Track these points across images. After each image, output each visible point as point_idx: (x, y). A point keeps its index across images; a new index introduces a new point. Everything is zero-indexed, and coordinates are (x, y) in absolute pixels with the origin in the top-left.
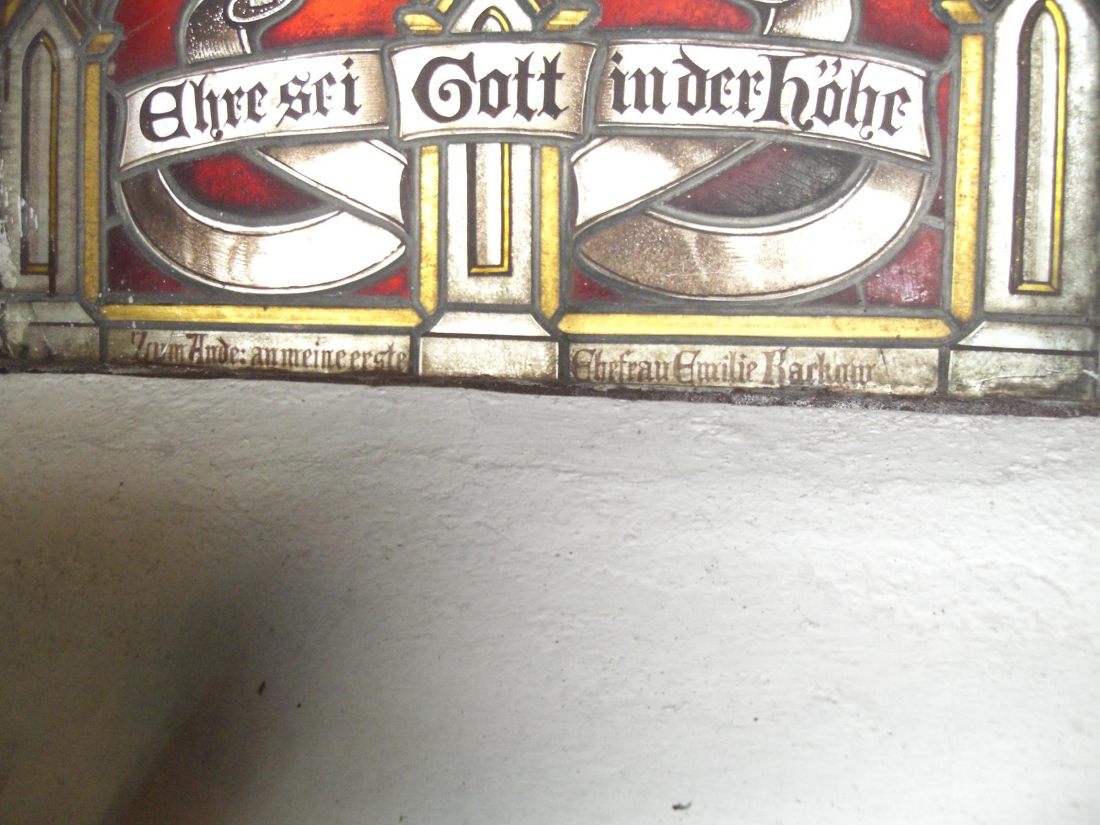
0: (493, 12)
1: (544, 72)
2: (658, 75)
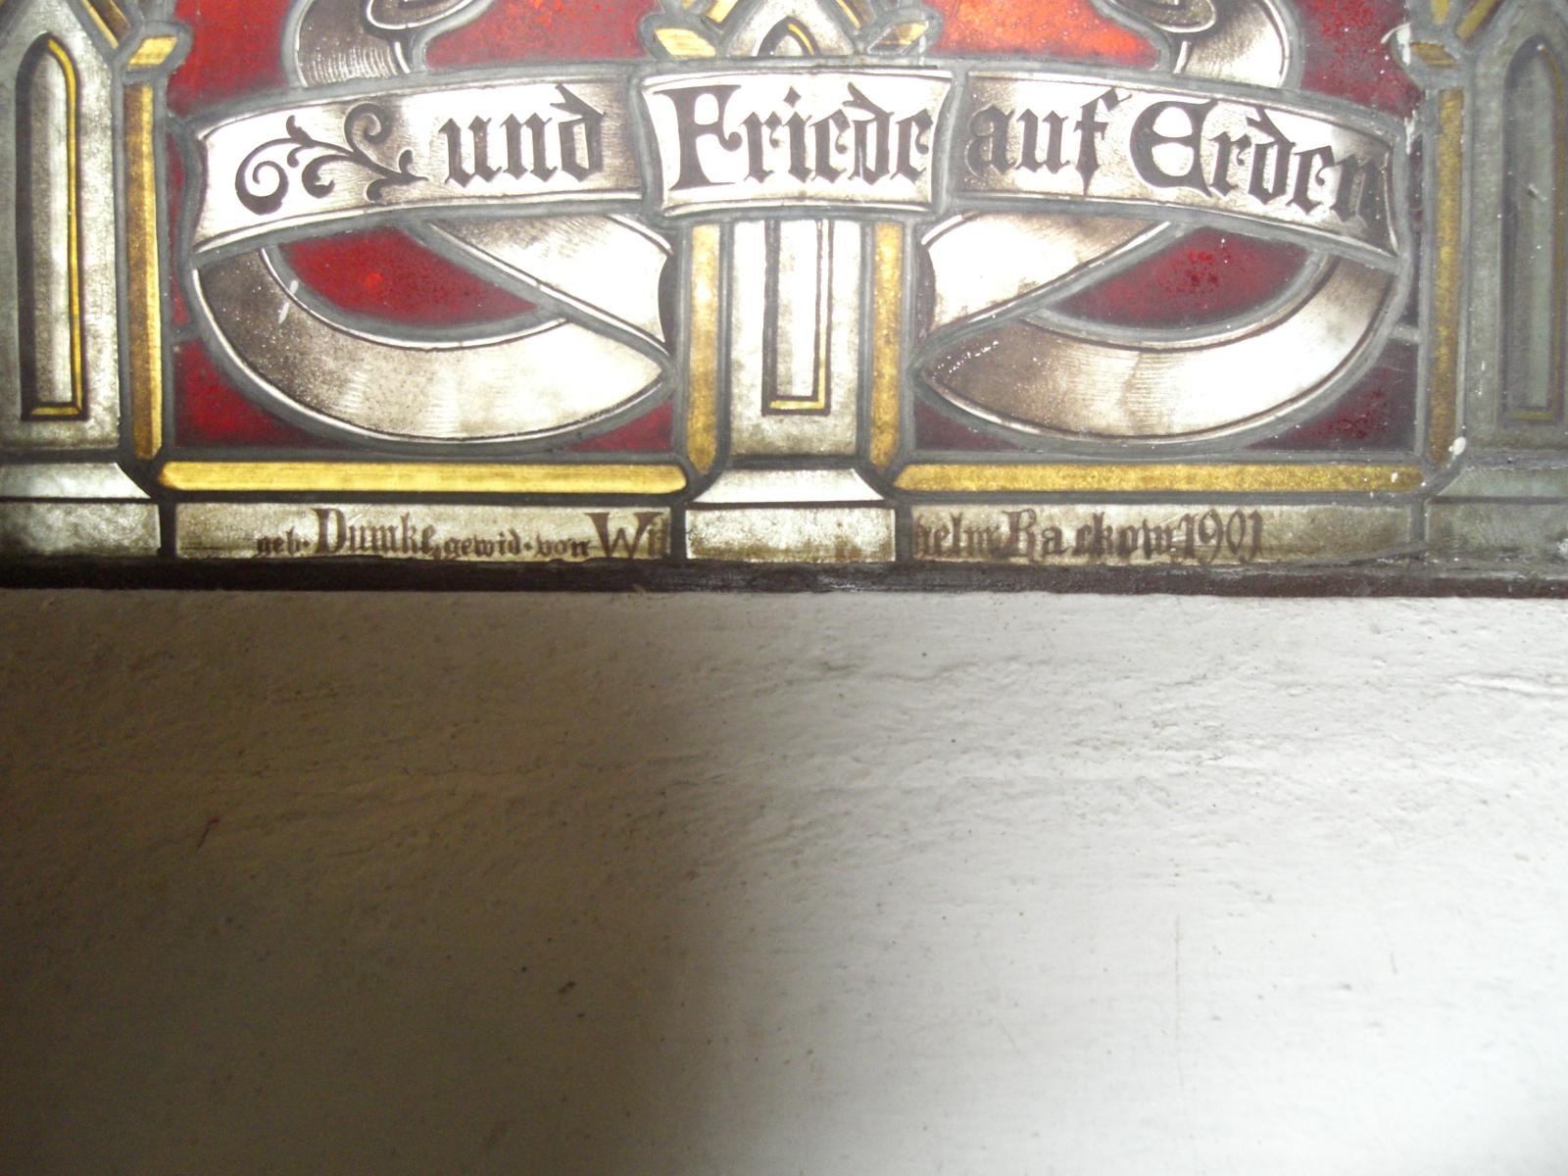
0: (793, 28)
1: (1080, 119)
2: (536, 124)
